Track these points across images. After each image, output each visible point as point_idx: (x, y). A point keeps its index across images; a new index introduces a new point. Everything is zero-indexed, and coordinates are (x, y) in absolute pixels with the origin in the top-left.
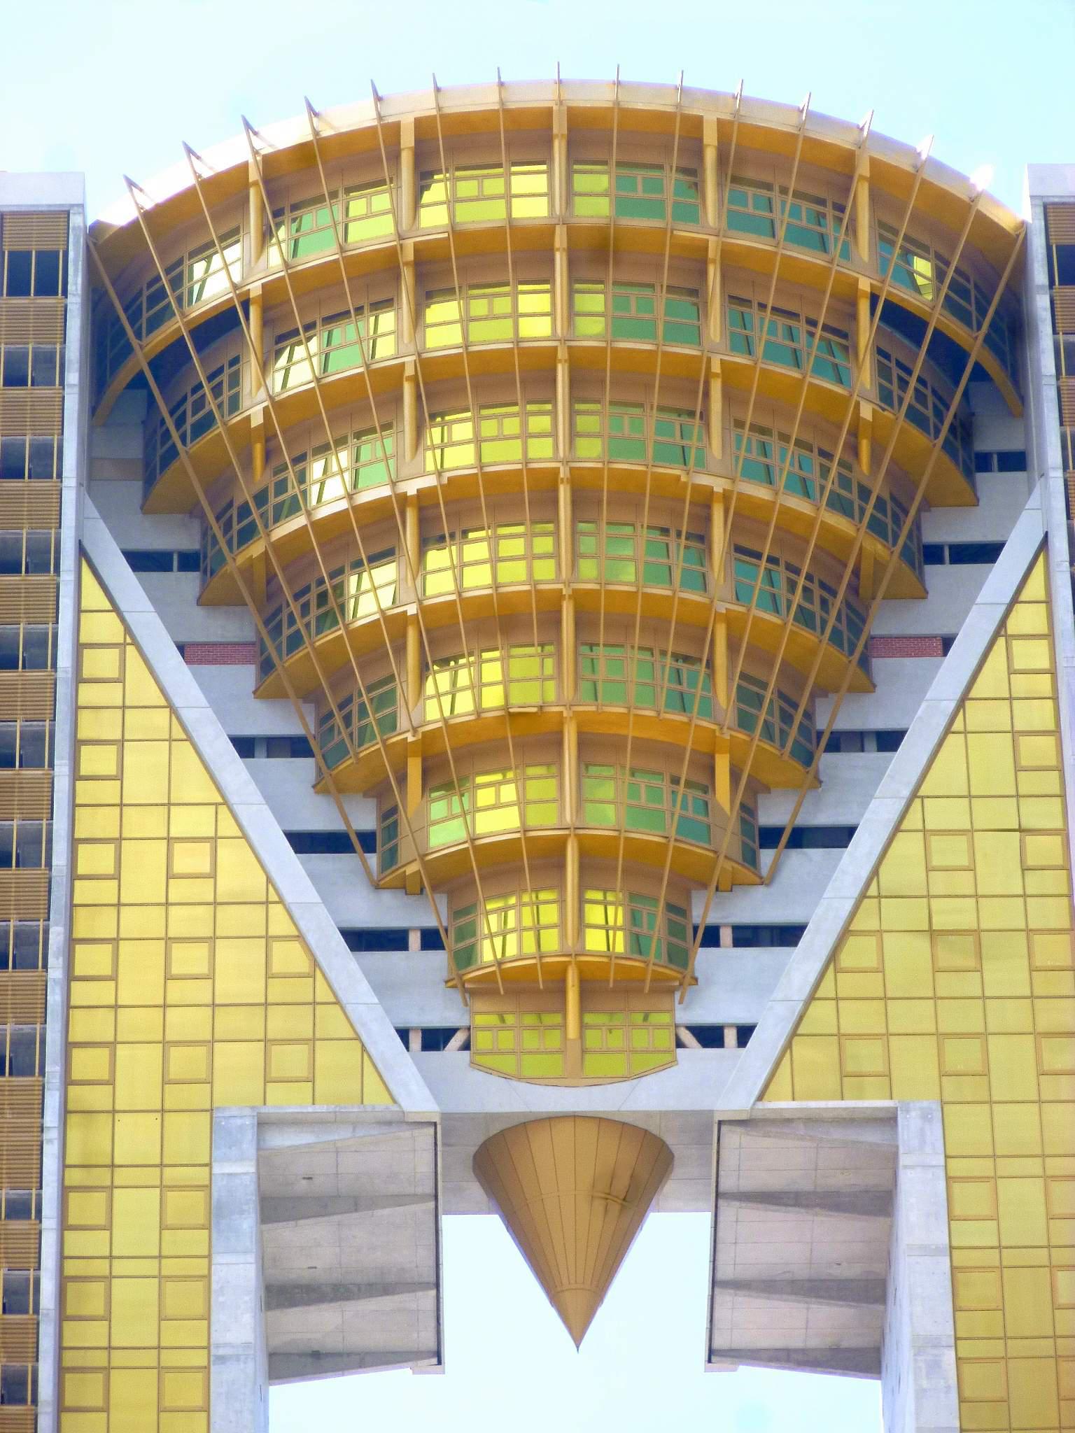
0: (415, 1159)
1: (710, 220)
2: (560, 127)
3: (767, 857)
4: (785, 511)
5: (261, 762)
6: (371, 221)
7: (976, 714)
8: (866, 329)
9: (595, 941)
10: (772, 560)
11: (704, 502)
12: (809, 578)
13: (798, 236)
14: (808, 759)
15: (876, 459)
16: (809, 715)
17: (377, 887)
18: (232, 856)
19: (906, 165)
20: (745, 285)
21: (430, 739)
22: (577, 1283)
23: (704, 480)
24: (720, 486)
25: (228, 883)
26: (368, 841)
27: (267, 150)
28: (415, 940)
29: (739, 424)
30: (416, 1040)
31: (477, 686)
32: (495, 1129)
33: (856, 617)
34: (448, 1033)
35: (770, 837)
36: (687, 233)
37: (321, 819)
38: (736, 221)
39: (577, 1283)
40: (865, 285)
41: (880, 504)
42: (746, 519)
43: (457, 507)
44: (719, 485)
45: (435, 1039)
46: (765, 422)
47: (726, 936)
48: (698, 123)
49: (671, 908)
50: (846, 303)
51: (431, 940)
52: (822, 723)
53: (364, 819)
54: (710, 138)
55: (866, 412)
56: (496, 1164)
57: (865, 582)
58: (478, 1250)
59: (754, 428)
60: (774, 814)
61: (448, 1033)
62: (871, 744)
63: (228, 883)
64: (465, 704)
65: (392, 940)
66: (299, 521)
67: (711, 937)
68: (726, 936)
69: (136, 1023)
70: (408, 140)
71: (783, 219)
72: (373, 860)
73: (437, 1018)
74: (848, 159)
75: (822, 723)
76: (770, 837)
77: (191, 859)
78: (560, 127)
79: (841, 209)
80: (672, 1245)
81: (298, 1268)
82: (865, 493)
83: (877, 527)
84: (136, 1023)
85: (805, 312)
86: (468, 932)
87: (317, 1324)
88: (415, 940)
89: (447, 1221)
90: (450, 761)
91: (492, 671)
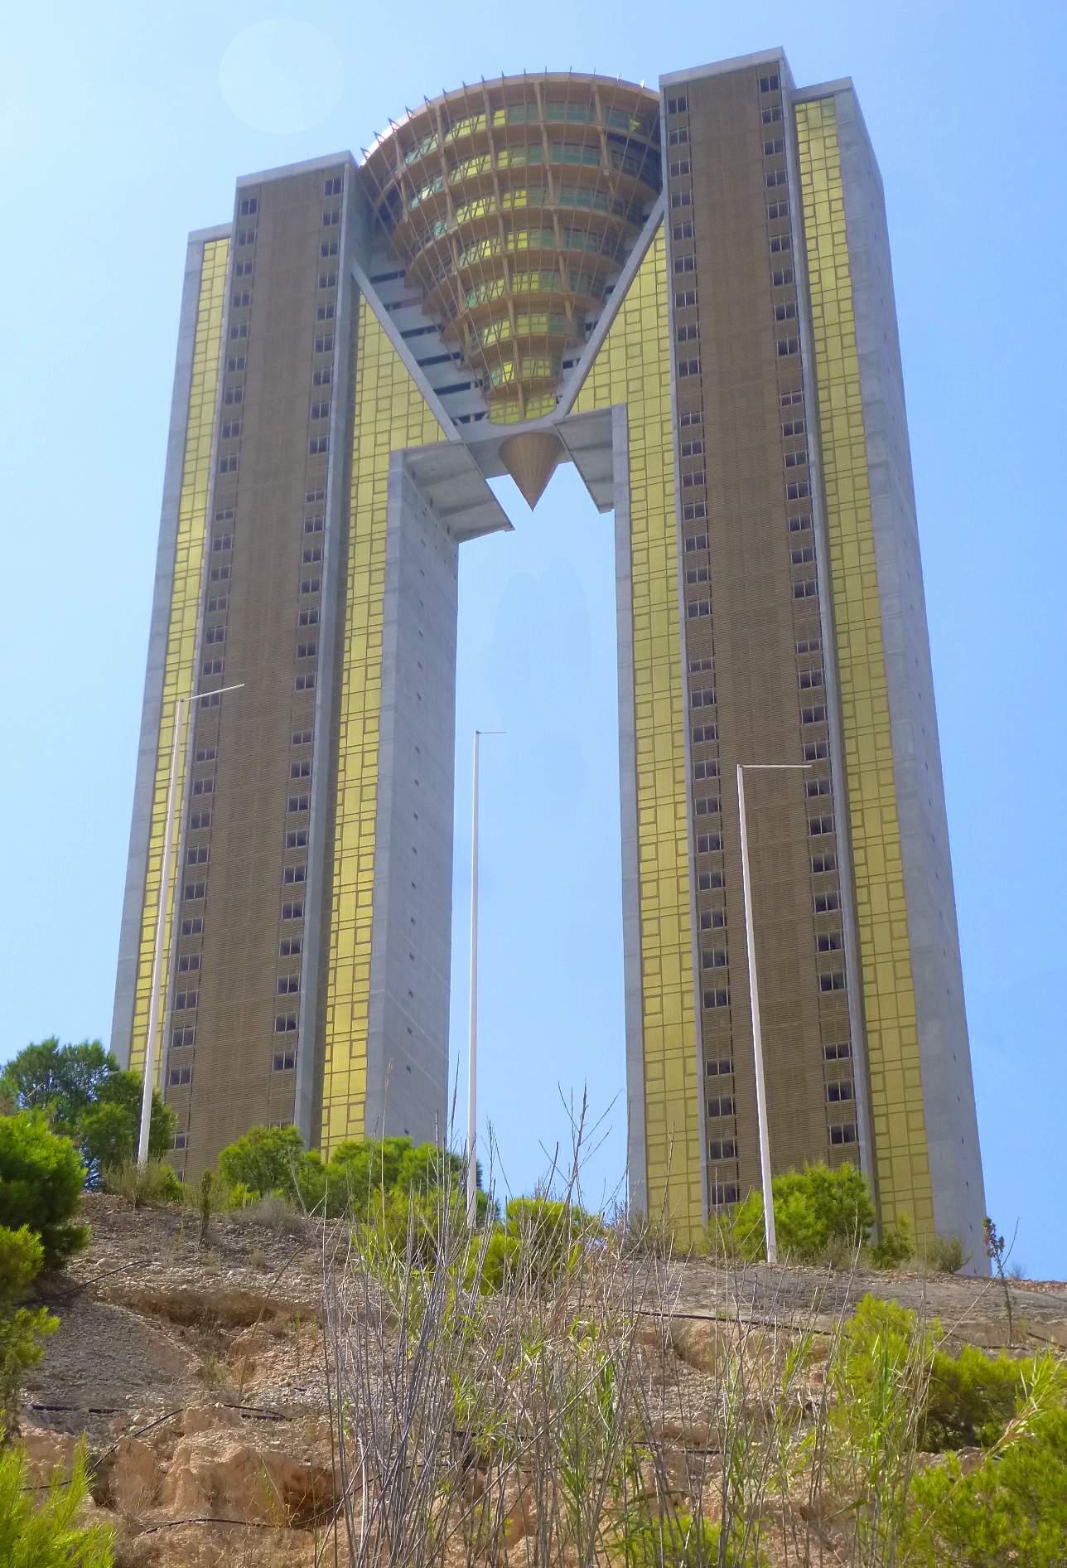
1: (541, 117)
2: (486, 97)
6: (432, 145)
7: (643, 269)
8: (603, 139)
9: (541, 372)
17: (460, 370)
18: (399, 367)
19: (610, 84)
20: (555, 135)
21: (466, 317)
24: (552, 208)
25: (396, 378)
31: (530, 282)
36: (532, 123)
42: (564, 217)
43: (488, 232)
48: (532, 85)
54: (537, 89)
55: (606, 173)
56: (503, 455)
63: (396, 378)
64: (525, 287)
66: (431, 243)
69: (828, 297)
70: (438, 113)
73: (479, 410)
74: (588, 87)
77: (384, 371)
80: (566, 477)
84: (828, 297)
86: (487, 378)
90: (482, 318)
91: (535, 277)
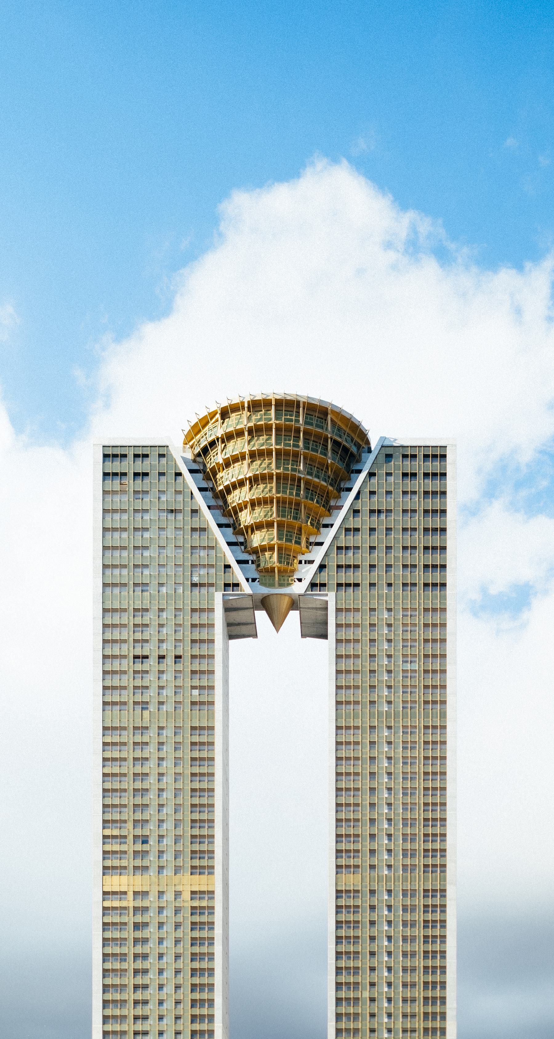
0: (249, 603)
3: (310, 547)
4: (322, 485)
5: (224, 529)
10: (312, 491)
11: (300, 479)
12: (319, 494)
13: (317, 426)
14: (318, 529)
15: (331, 471)
16: (319, 520)
22: (277, 621)
23: (300, 475)
26: (242, 544)
27: (222, 406)
28: (250, 562)
29: (306, 464)
30: (250, 580)
32: (264, 596)
33: (327, 502)
34: (256, 579)
35: (311, 544)
37: (233, 539)
38: (306, 423)
39: (277, 621)
40: (329, 436)
41: (332, 479)
44: (302, 476)
45: (254, 580)
46: (311, 463)
47: (303, 562)
49: (307, 538)
50: (326, 439)
51: (253, 562)
52: (342, 486)
53: (241, 539)
55: (329, 461)
56: (264, 603)
57: (330, 495)
58: (261, 616)
59: (309, 464)
60: (312, 540)
61: (256, 579)
62: (330, 526)
65: (246, 562)
67: (300, 562)
68: (303, 562)
71: (314, 422)
72: (243, 547)
75: (342, 486)
76: (311, 544)
78: (273, 403)
79: (326, 420)
80: (294, 617)
81: (232, 621)
82: (329, 477)
83: (331, 485)
85: (319, 441)
87: (236, 630)
88: (250, 562)
89: (255, 612)
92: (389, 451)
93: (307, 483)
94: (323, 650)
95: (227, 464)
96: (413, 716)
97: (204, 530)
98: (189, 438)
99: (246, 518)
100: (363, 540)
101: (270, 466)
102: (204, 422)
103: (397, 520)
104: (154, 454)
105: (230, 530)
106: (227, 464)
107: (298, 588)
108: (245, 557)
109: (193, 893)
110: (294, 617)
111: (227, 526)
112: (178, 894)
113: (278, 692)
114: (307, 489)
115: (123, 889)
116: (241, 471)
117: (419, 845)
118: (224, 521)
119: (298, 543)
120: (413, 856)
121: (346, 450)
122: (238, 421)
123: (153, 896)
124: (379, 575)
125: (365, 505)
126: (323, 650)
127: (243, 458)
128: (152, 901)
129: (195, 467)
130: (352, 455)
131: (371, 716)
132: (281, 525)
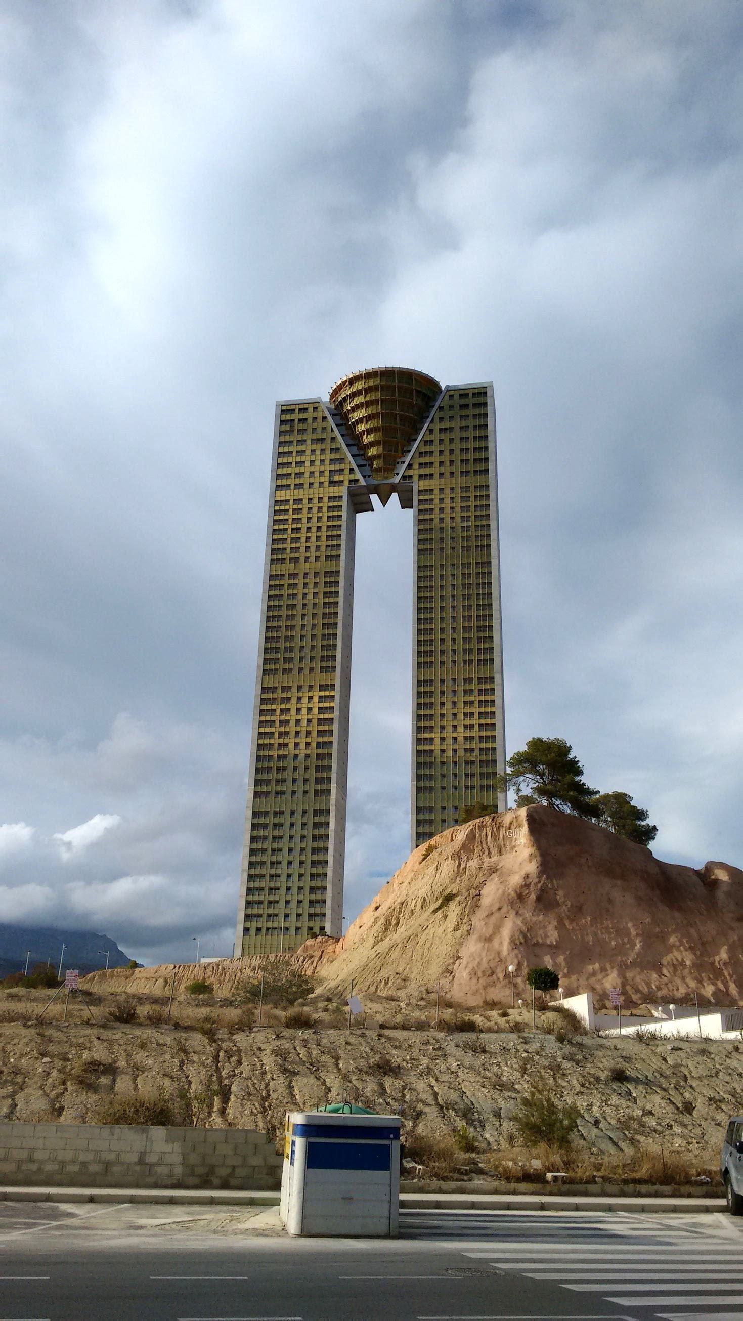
0: (365, 491)
22: (384, 501)
26: (362, 455)
38: (399, 382)
39: (384, 501)
53: (362, 453)
56: (375, 490)
58: (374, 499)
65: (365, 466)
80: (395, 497)
92: (452, 393)
93: (400, 416)
94: (410, 514)
95: (354, 409)
96: (468, 556)
97: (338, 449)
98: (332, 396)
99: (366, 439)
100: (436, 448)
101: (378, 395)
102: (340, 388)
103: (457, 434)
104: (311, 410)
105: (355, 448)
106: (354, 409)
107: (397, 479)
108: (362, 463)
109: (329, 498)
110: (395, 497)
111: (354, 445)
112: (320, 499)
113: (385, 538)
114: (401, 420)
115: (287, 498)
116: (361, 413)
117: (474, 634)
118: (351, 442)
119: (396, 451)
120: (469, 588)
121: (424, 394)
122: (359, 385)
123: (305, 501)
124: (447, 469)
125: (437, 426)
126: (410, 514)
127: (362, 406)
128: (305, 505)
129: (336, 412)
130: (429, 398)
131: (441, 557)
132: (385, 443)
